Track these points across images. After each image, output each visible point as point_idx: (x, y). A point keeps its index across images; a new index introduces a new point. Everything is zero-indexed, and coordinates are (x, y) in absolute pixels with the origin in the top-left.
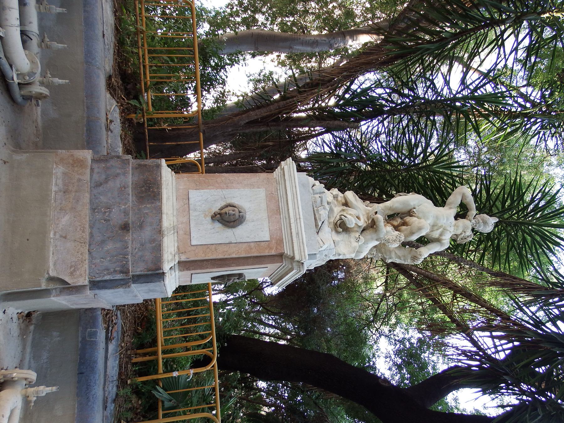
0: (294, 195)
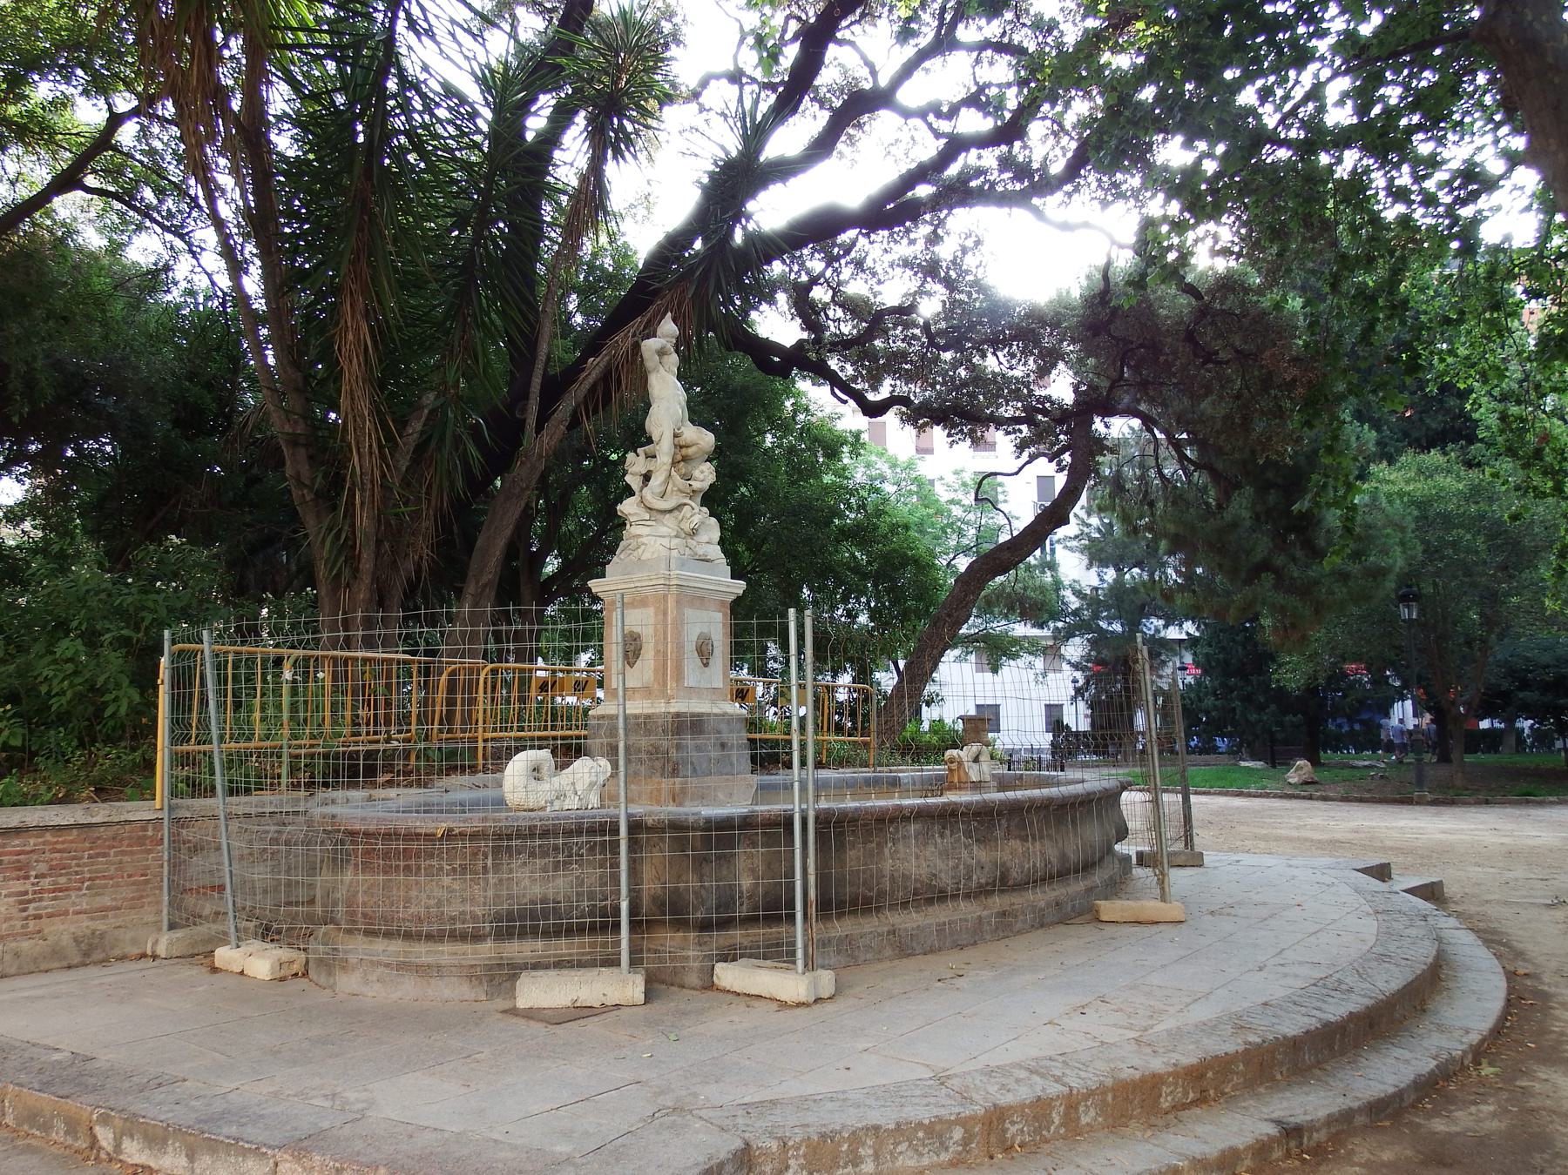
0: (703, 580)
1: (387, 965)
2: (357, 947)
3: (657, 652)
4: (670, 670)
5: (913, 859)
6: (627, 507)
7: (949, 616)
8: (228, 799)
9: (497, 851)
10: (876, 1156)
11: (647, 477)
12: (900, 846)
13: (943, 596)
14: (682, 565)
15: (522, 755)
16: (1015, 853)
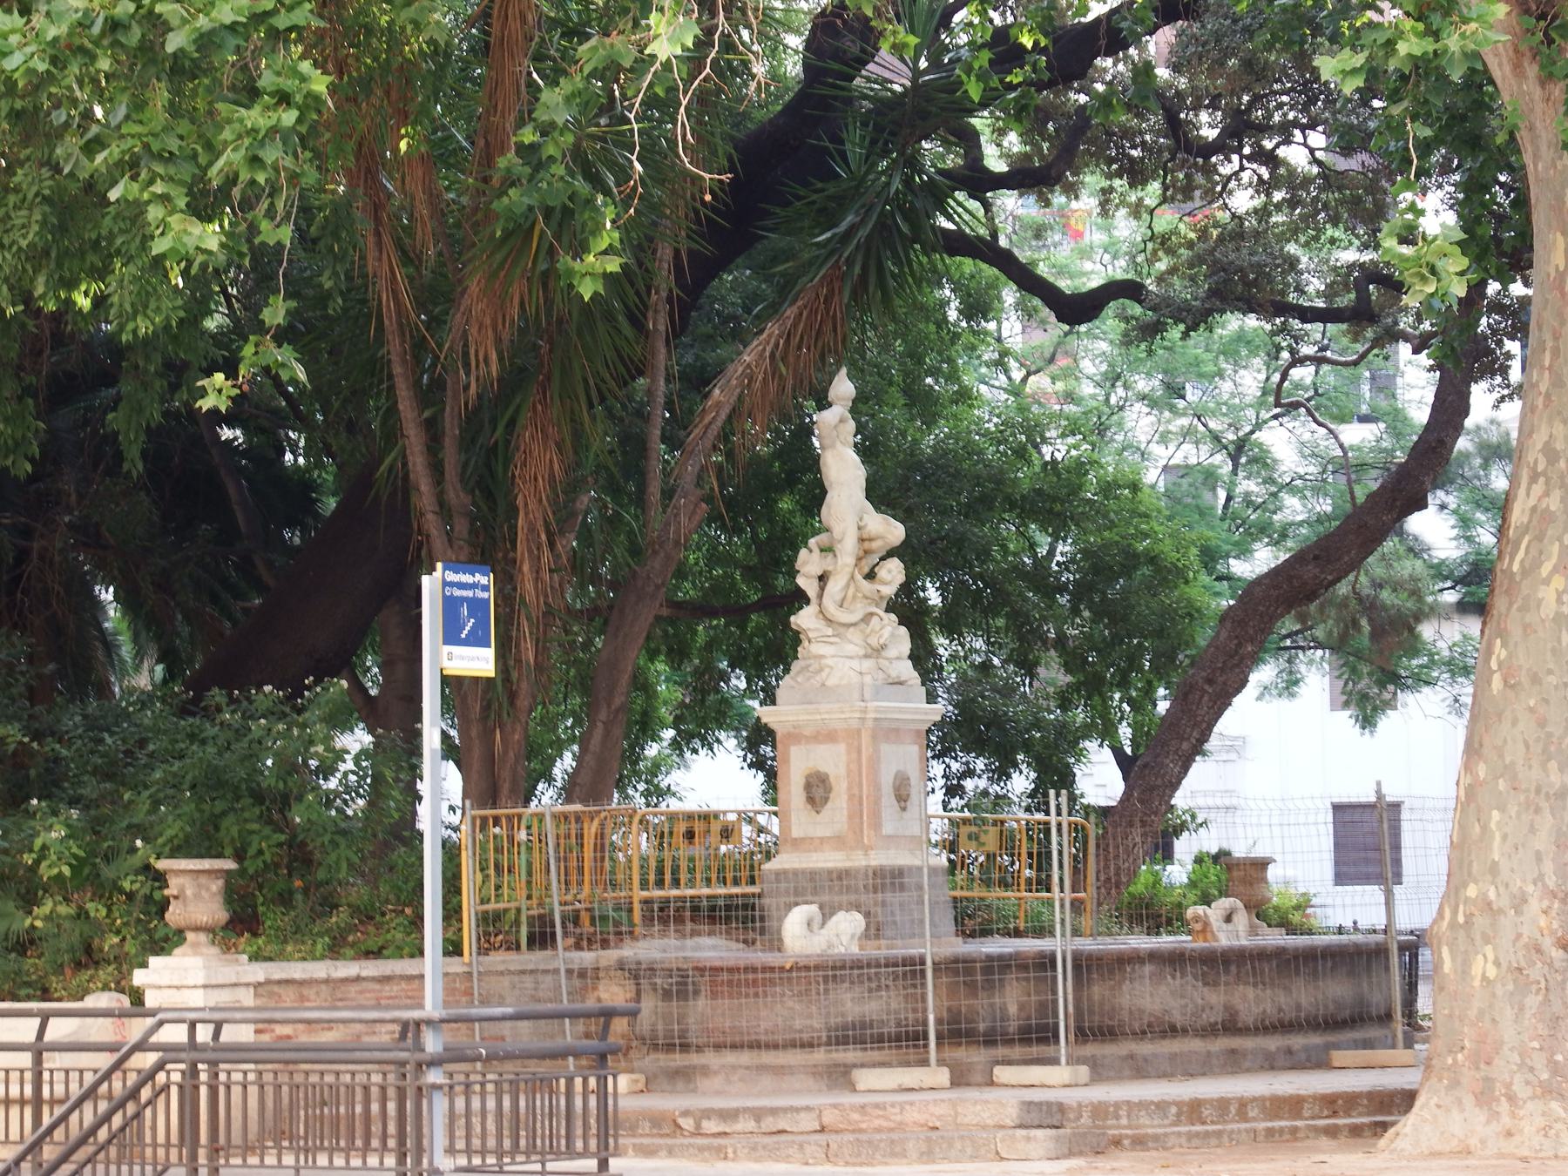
0: (901, 710)
1: (747, 1068)
2: (710, 1058)
3: (851, 797)
4: (863, 816)
5: (1147, 996)
6: (804, 619)
7: (1210, 681)
8: (481, 958)
9: (826, 978)
10: (1129, 1116)
11: (823, 578)
12: (1137, 985)
13: (1203, 637)
14: (877, 695)
15: (796, 910)
16: (1251, 1000)
